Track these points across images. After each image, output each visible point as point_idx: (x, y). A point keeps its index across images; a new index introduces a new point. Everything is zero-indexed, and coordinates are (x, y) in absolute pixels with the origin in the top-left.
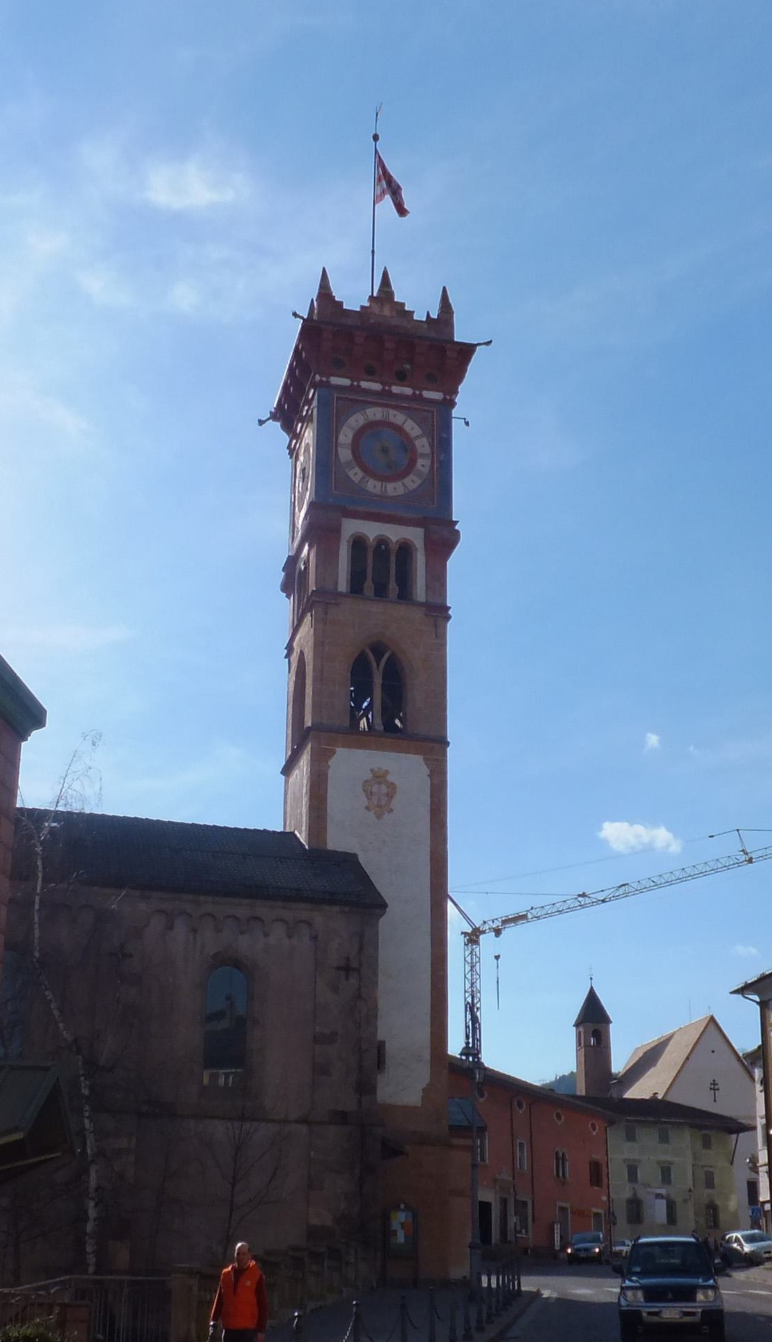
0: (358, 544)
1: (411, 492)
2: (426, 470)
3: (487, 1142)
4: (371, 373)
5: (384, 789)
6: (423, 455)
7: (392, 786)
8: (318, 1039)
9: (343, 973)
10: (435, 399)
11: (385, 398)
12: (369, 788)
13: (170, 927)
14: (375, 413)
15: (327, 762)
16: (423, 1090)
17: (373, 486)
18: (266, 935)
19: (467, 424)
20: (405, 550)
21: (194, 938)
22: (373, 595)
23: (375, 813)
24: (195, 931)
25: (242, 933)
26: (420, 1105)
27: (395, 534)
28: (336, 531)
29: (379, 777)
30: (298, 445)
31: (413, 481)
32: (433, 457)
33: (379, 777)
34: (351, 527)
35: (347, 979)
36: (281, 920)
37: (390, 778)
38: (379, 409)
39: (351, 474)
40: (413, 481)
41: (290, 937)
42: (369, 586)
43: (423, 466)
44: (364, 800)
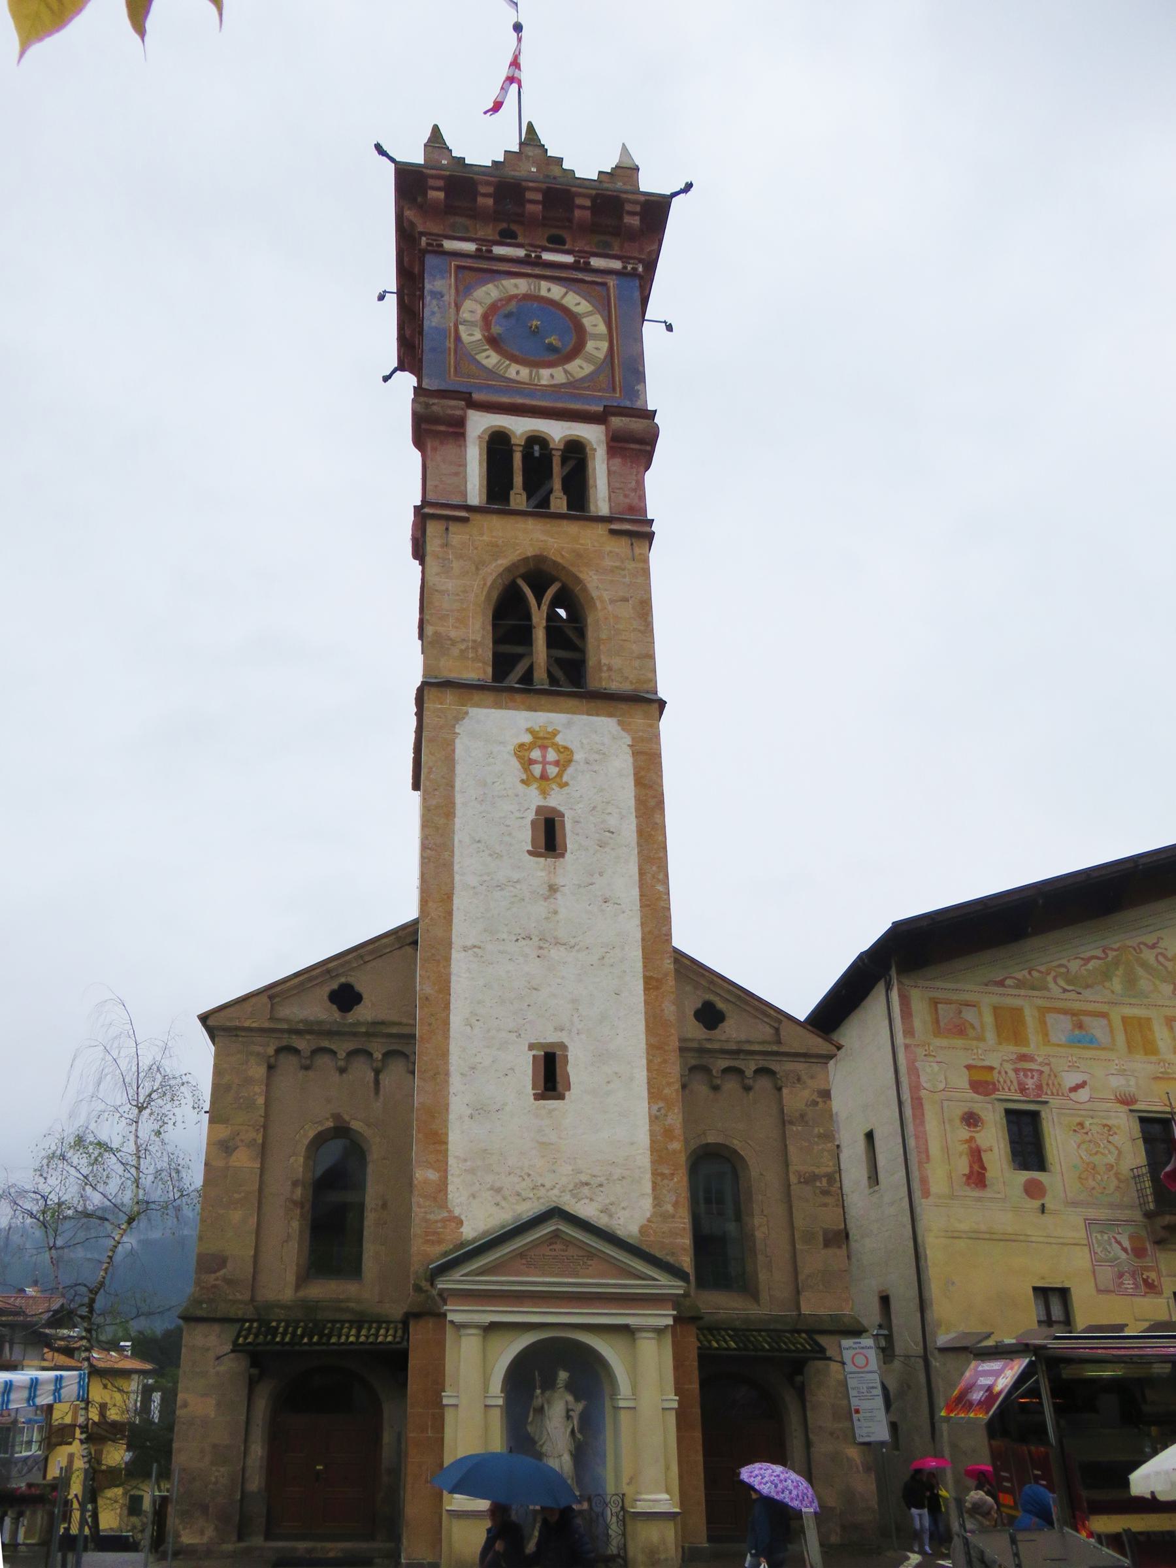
1: (577, 381)
2: (601, 355)
5: (552, 755)
6: (597, 337)
10: (614, 261)
11: (532, 266)
14: (520, 286)
19: (669, 328)
20: (576, 451)
27: (557, 431)
28: (456, 430)
29: (542, 740)
30: (442, 428)
31: (581, 367)
40: (581, 367)
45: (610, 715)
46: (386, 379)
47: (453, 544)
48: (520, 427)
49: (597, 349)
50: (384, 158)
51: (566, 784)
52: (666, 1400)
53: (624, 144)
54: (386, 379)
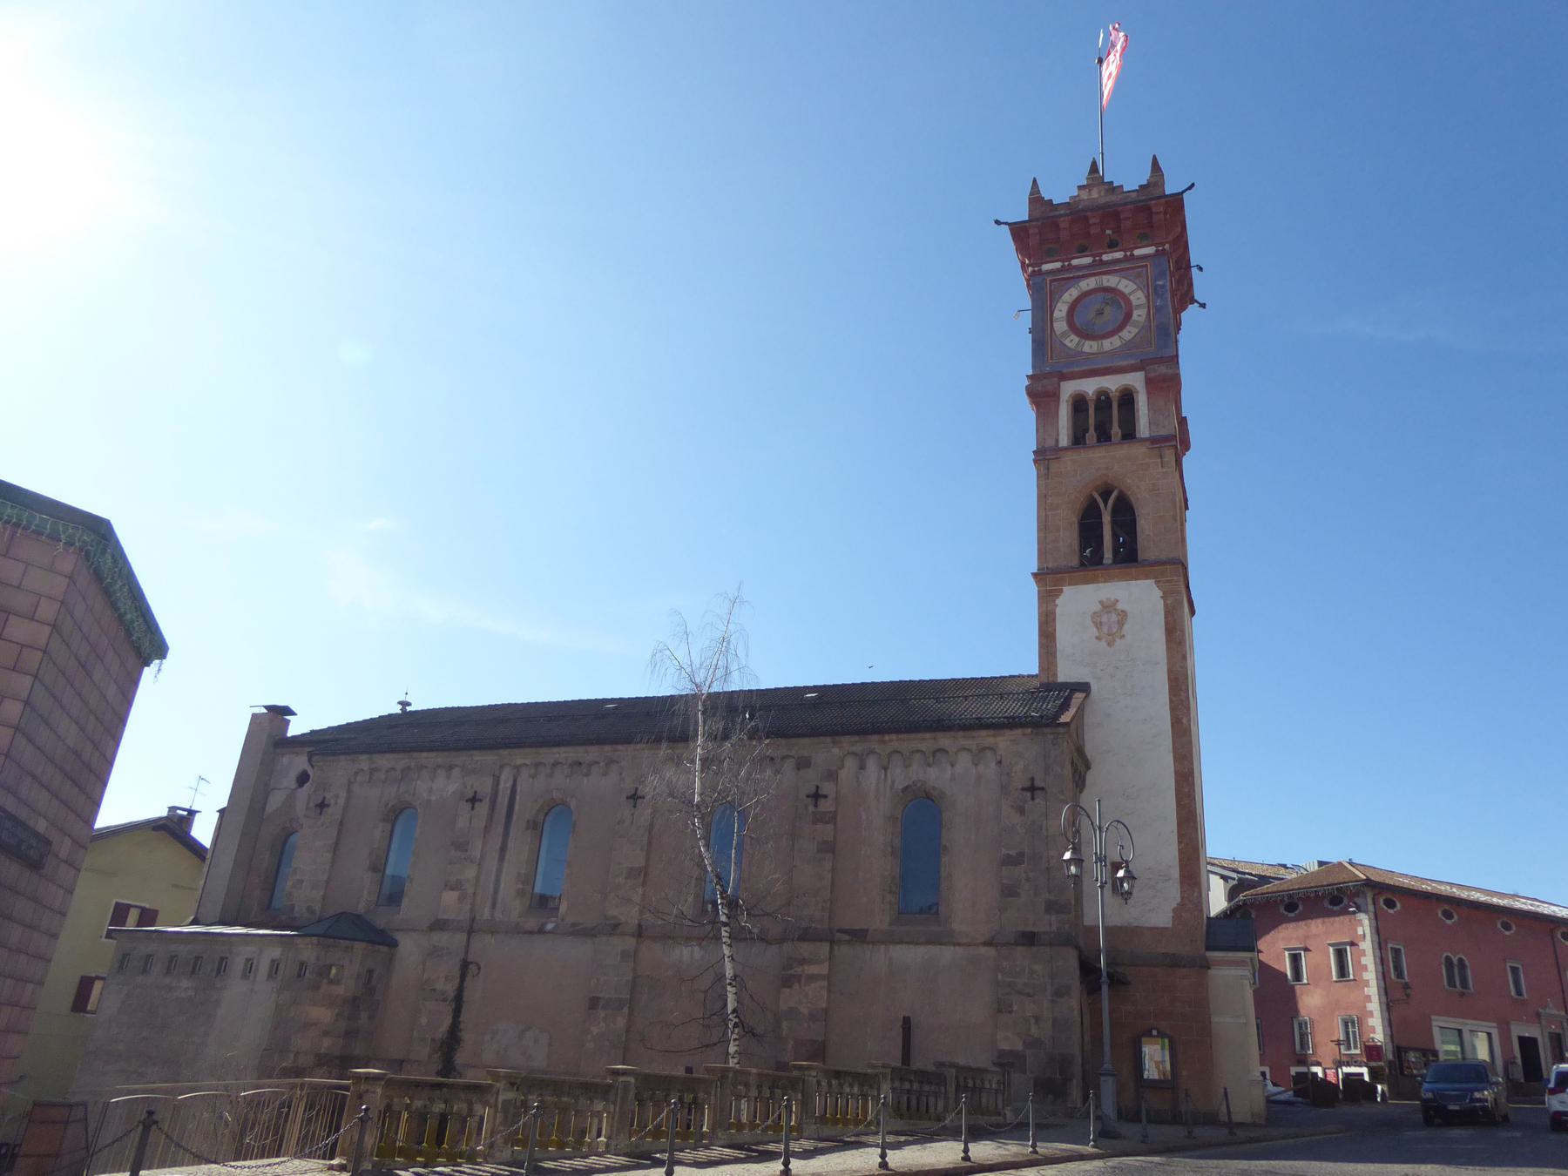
2: (1142, 319)
3: (1522, 975)
4: (1082, 250)
6: (1138, 307)
7: (1123, 615)
8: (1009, 861)
9: (1028, 794)
11: (1099, 268)
12: (1099, 619)
13: (862, 767)
15: (1054, 601)
16: (1173, 910)
17: (1090, 347)
18: (952, 765)
21: (886, 775)
22: (1095, 441)
23: (1106, 641)
24: (885, 769)
25: (929, 765)
26: (1170, 926)
27: (1113, 383)
28: (1055, 395)
29: (1108, 607)
32: (1149, 307)
33: (1108, 607)
34: (1069, 389)
35: (1033, 799)
36: (965, 749)
37: (1120, 606)
38: (1093, 279)
39: (1067, 342)
41: (976, 765)
42: (1091, 435)
43: (1139, 316)
44: (1094, 631)
45: (1147, 578)
46: (998, 222)
47: (1020, 948)
48: (1090, 386)
49: (1138, 299)
50: (1002, 225)
51: (1123, 636)
52: (391, 835)
53: (1154, 156)
54: (998, 222)
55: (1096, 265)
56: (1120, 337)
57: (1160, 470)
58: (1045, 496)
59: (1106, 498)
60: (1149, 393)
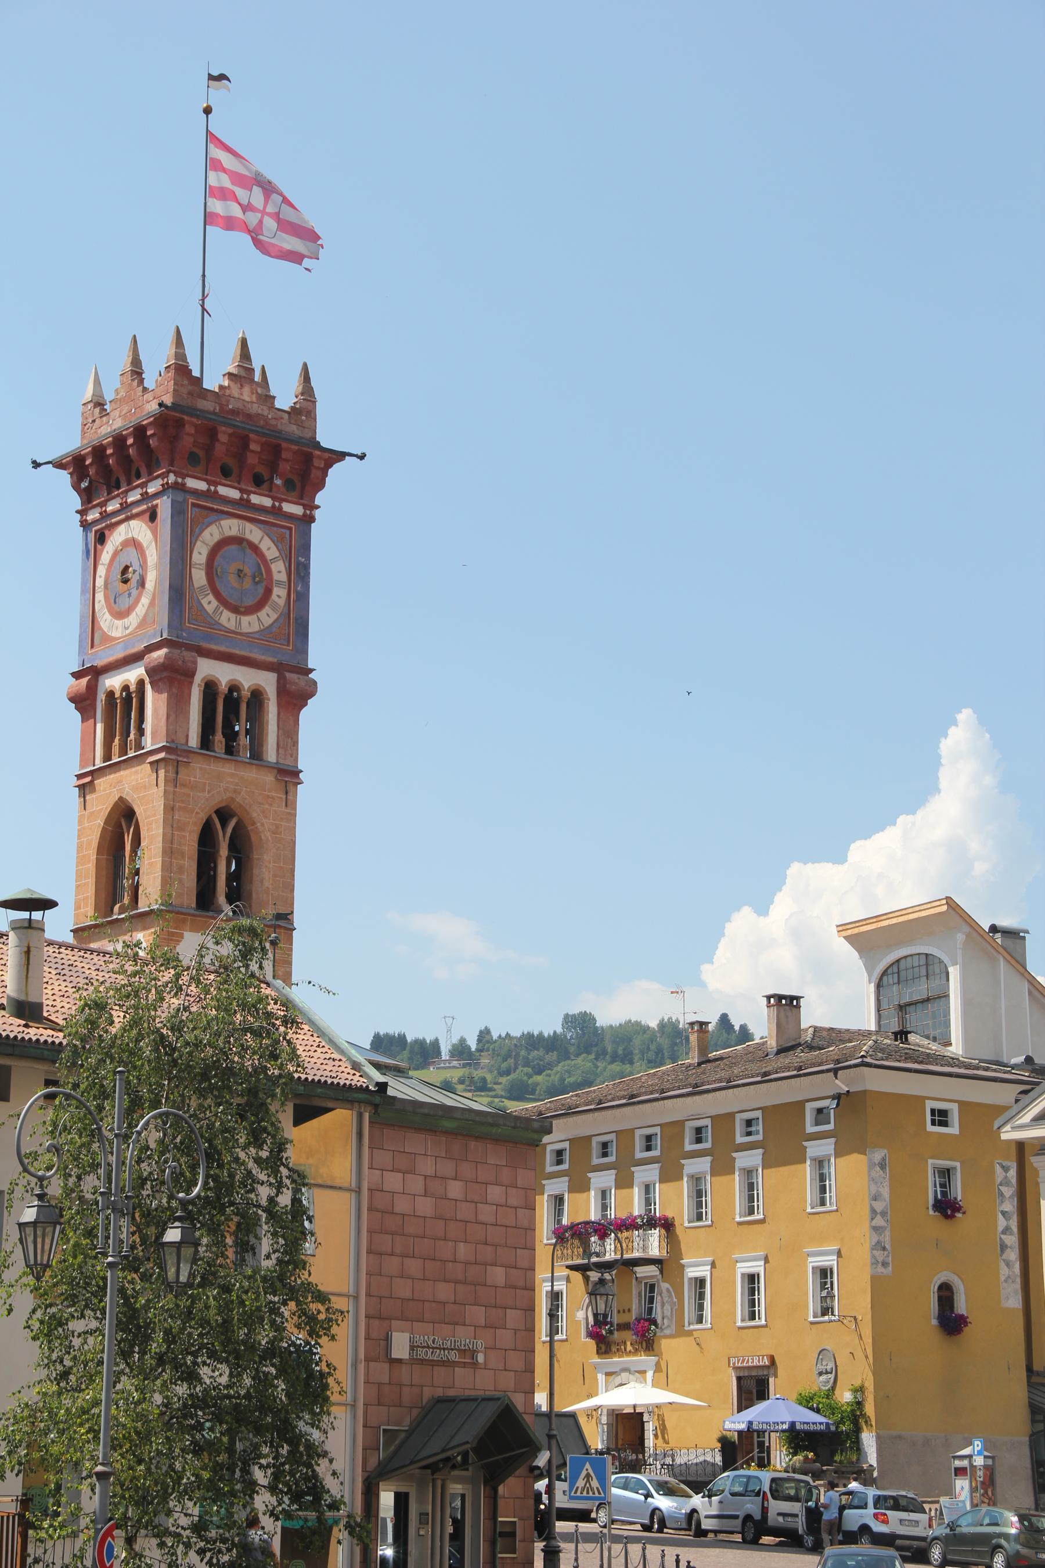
0: (210, 688)
11: (243, 509)
20: (257, 697)
27: (247, 678)
34: (206, 668)
38: (234, 522)
55: (242, 505)
56: (259, 619)
57: (284, 809)
58: (173, 809)
59: (224, 824)
60: (280, 705)
